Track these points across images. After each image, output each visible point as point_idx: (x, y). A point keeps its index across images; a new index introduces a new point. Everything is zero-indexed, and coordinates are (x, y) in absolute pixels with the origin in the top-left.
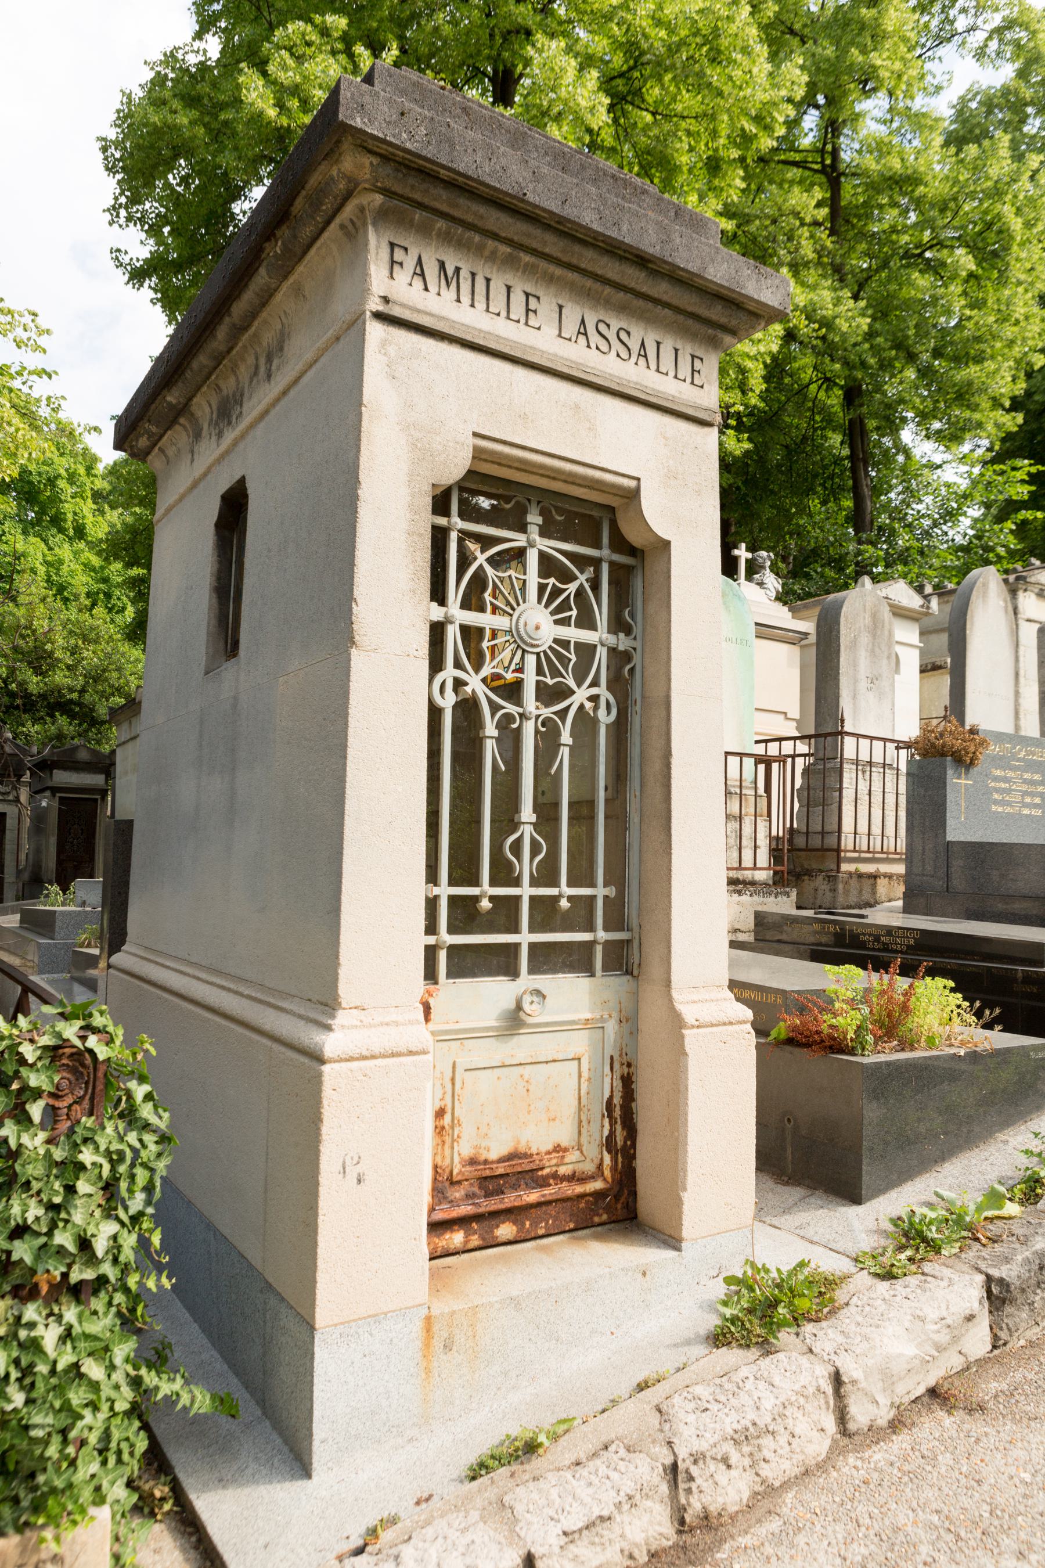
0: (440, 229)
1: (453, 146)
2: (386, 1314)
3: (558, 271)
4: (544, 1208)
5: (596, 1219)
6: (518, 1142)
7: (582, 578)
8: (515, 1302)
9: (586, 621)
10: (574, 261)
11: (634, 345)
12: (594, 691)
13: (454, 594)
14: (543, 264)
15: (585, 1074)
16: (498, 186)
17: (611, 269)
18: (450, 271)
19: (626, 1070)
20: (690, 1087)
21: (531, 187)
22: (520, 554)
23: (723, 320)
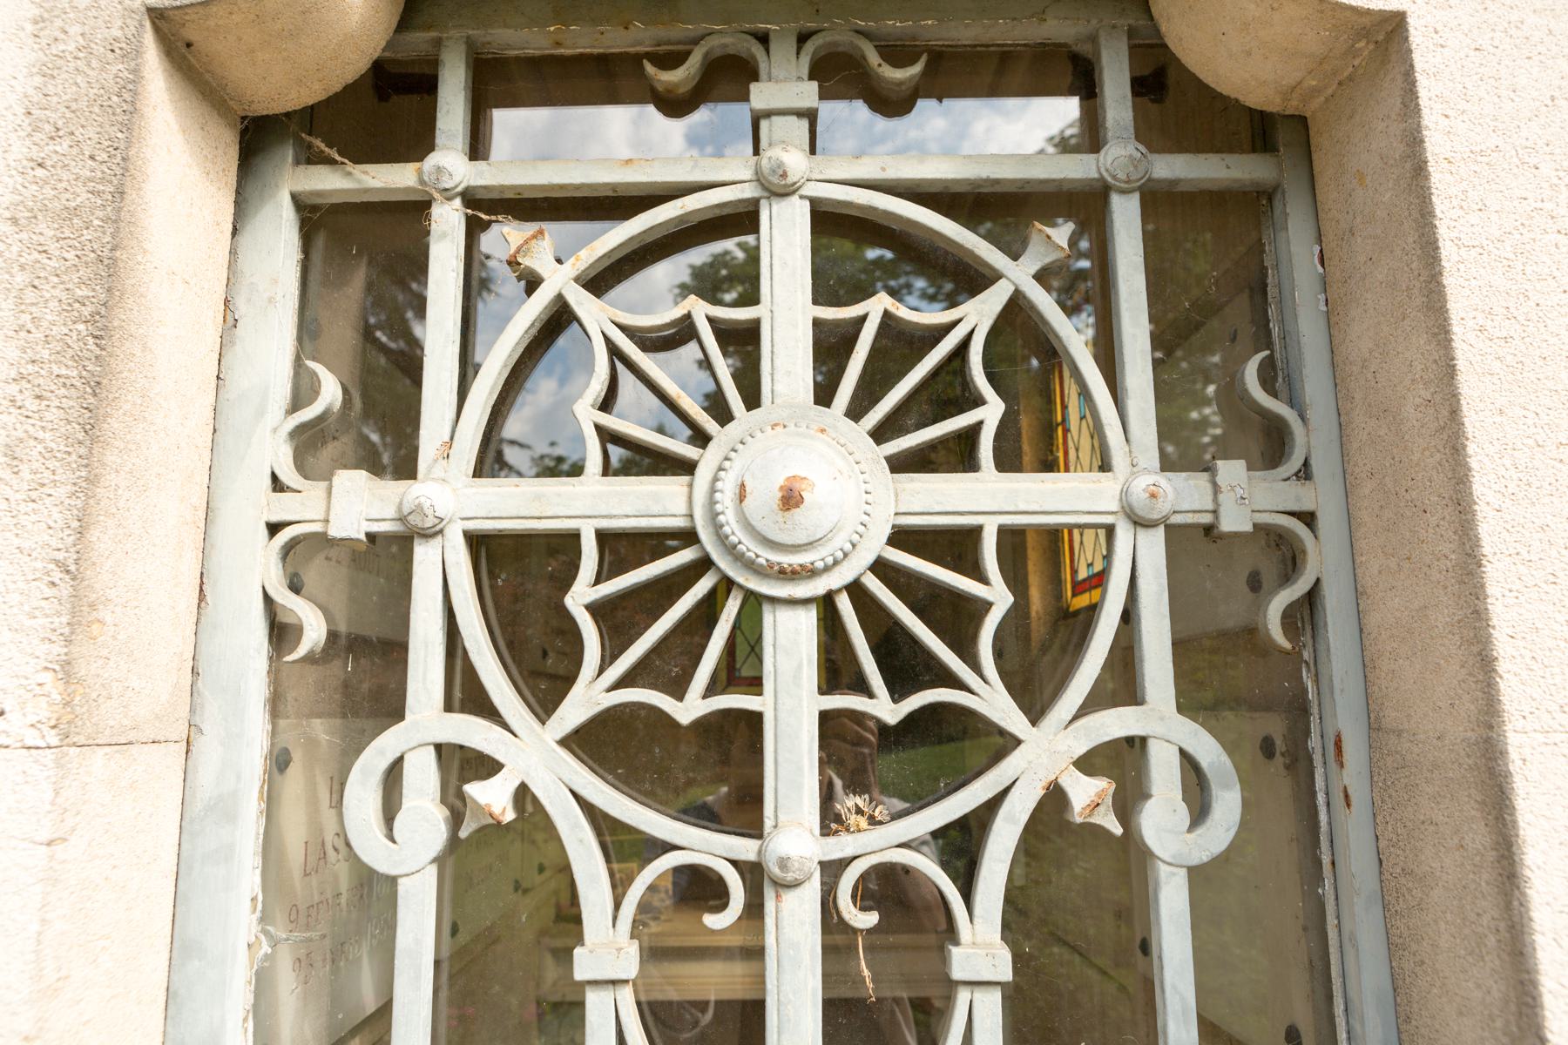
12: (1115, 723)
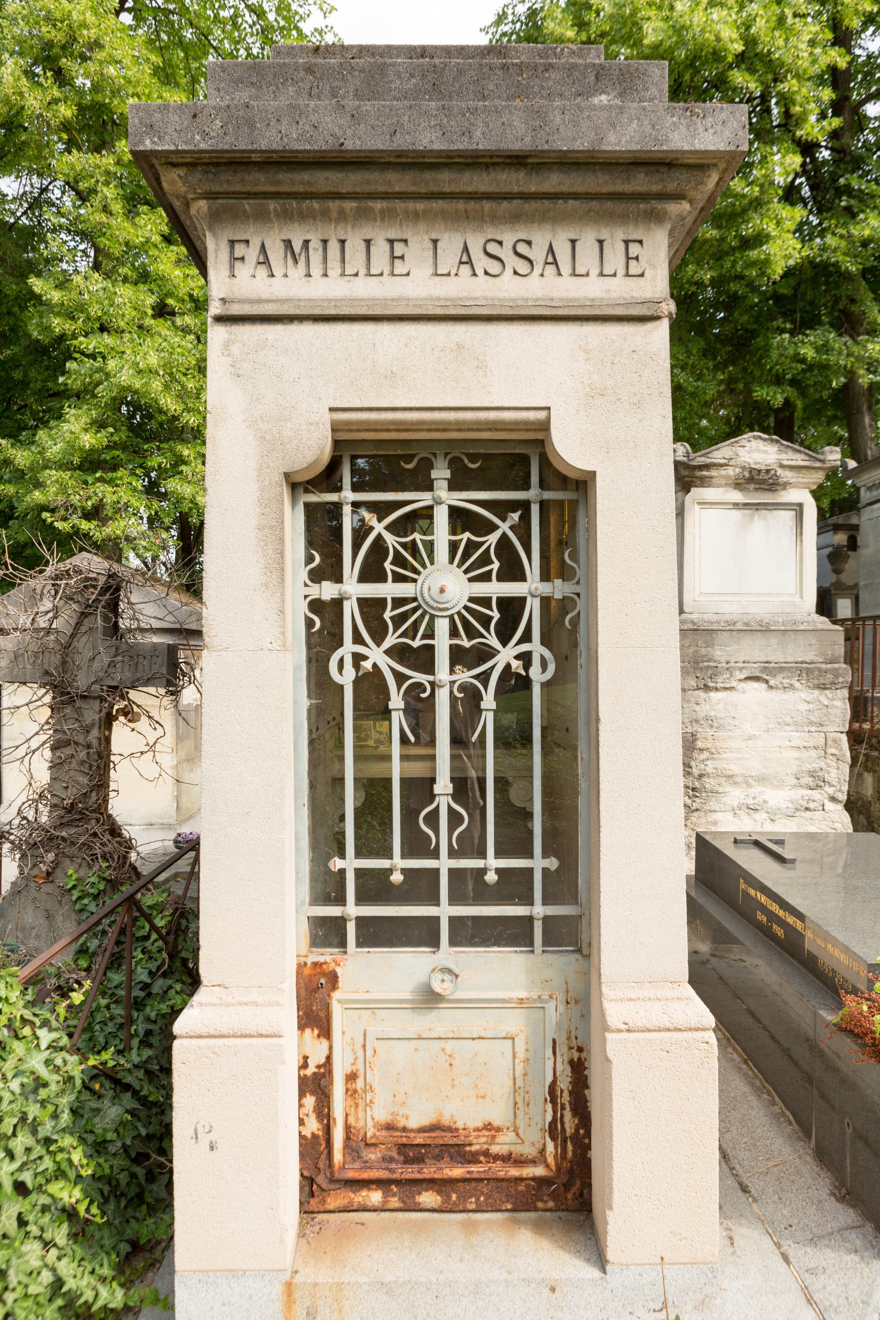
0: (275, 210)
1: (252, 127)
2: (245, 1271)
3: (420, 206)
4: (474, 1184)
5: (540, 1205)
6: (441, 1115)
7: (504, 527)
8: (388, 1288)
9: (513, 571)
10: (435, 189)
11: (538, 254)
12: (524, 647)
13: (351, 568)
14: (399, 205)
15: (521, 1055)
16: (308, 147)
17: (481, 182)
18: (297, 246)
19: (576, 1055)
20: (614, 1098)
21: (349, 132)
22: (427, 513)
23: (655, 188)
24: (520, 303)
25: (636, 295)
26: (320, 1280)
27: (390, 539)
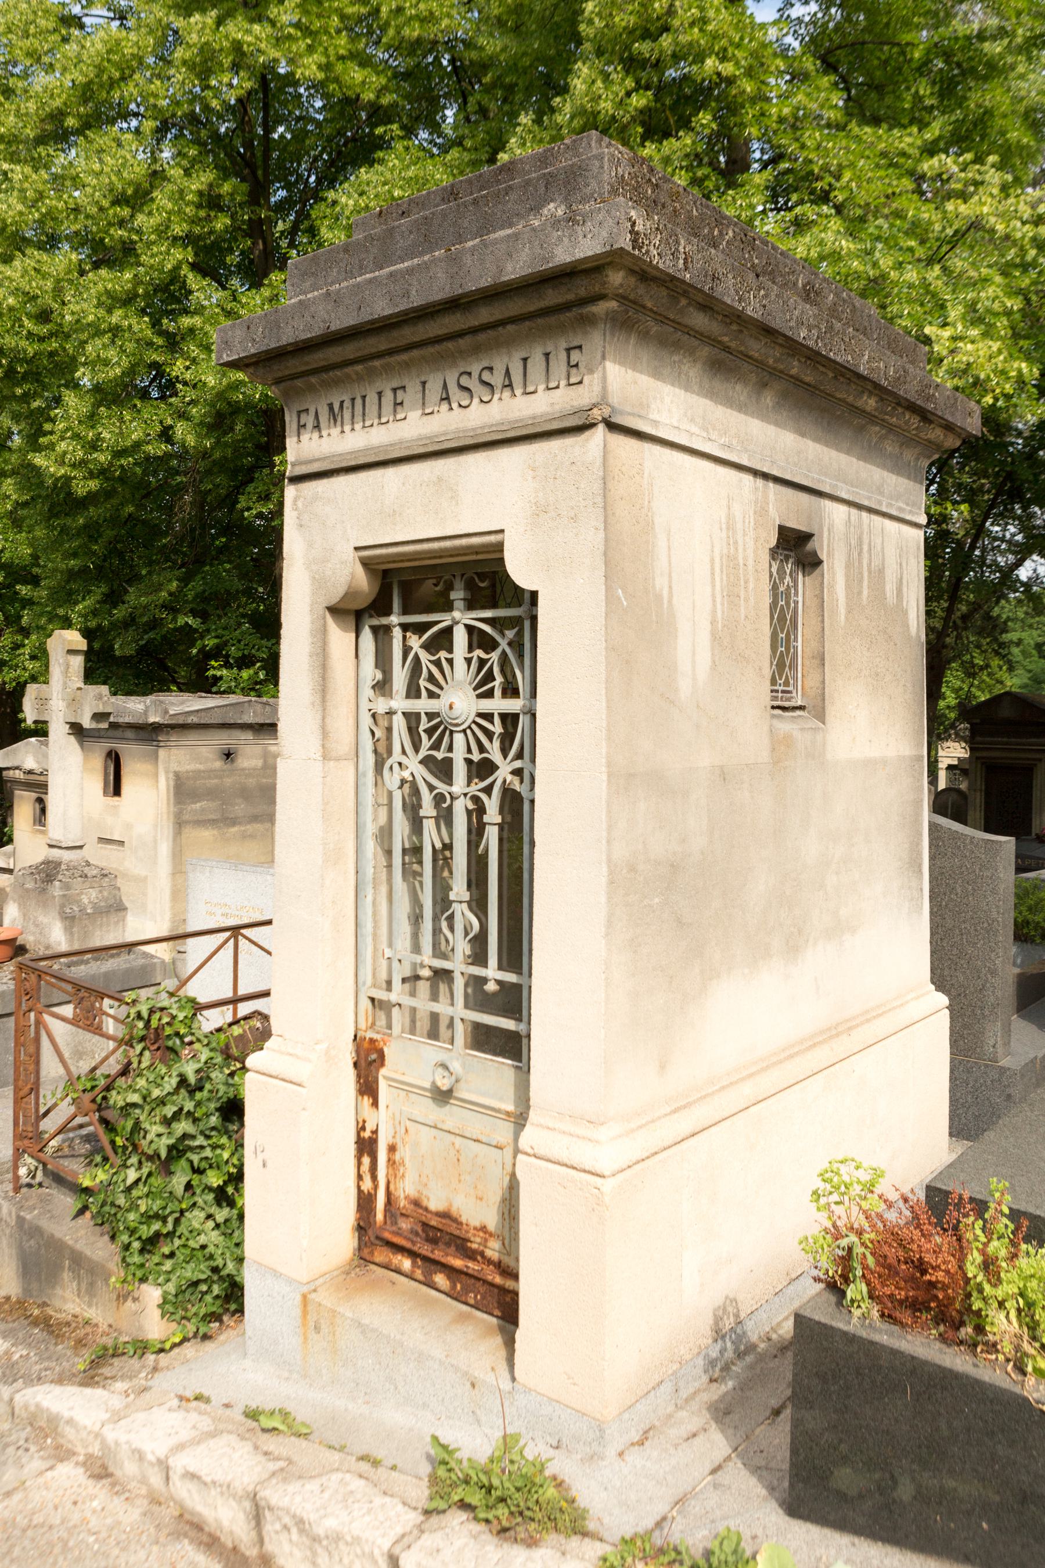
6: (451, 1205)
11: (497, 379)
12: (518, 764)
22: (448, 631)
23: (570, 297)
24: (479, 431)
25: (575, 403)
26: (324, 1302)
27: (424, 657)
